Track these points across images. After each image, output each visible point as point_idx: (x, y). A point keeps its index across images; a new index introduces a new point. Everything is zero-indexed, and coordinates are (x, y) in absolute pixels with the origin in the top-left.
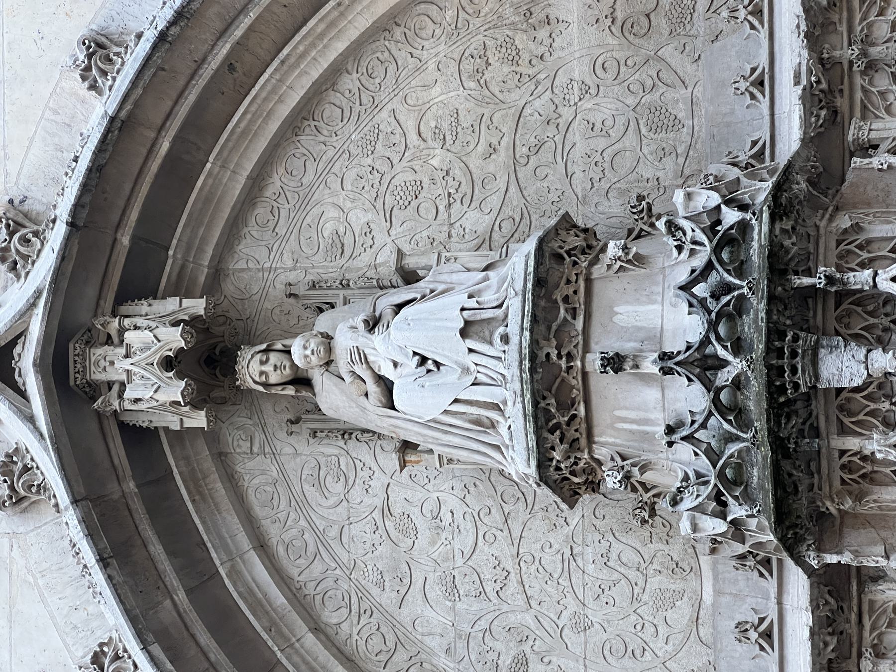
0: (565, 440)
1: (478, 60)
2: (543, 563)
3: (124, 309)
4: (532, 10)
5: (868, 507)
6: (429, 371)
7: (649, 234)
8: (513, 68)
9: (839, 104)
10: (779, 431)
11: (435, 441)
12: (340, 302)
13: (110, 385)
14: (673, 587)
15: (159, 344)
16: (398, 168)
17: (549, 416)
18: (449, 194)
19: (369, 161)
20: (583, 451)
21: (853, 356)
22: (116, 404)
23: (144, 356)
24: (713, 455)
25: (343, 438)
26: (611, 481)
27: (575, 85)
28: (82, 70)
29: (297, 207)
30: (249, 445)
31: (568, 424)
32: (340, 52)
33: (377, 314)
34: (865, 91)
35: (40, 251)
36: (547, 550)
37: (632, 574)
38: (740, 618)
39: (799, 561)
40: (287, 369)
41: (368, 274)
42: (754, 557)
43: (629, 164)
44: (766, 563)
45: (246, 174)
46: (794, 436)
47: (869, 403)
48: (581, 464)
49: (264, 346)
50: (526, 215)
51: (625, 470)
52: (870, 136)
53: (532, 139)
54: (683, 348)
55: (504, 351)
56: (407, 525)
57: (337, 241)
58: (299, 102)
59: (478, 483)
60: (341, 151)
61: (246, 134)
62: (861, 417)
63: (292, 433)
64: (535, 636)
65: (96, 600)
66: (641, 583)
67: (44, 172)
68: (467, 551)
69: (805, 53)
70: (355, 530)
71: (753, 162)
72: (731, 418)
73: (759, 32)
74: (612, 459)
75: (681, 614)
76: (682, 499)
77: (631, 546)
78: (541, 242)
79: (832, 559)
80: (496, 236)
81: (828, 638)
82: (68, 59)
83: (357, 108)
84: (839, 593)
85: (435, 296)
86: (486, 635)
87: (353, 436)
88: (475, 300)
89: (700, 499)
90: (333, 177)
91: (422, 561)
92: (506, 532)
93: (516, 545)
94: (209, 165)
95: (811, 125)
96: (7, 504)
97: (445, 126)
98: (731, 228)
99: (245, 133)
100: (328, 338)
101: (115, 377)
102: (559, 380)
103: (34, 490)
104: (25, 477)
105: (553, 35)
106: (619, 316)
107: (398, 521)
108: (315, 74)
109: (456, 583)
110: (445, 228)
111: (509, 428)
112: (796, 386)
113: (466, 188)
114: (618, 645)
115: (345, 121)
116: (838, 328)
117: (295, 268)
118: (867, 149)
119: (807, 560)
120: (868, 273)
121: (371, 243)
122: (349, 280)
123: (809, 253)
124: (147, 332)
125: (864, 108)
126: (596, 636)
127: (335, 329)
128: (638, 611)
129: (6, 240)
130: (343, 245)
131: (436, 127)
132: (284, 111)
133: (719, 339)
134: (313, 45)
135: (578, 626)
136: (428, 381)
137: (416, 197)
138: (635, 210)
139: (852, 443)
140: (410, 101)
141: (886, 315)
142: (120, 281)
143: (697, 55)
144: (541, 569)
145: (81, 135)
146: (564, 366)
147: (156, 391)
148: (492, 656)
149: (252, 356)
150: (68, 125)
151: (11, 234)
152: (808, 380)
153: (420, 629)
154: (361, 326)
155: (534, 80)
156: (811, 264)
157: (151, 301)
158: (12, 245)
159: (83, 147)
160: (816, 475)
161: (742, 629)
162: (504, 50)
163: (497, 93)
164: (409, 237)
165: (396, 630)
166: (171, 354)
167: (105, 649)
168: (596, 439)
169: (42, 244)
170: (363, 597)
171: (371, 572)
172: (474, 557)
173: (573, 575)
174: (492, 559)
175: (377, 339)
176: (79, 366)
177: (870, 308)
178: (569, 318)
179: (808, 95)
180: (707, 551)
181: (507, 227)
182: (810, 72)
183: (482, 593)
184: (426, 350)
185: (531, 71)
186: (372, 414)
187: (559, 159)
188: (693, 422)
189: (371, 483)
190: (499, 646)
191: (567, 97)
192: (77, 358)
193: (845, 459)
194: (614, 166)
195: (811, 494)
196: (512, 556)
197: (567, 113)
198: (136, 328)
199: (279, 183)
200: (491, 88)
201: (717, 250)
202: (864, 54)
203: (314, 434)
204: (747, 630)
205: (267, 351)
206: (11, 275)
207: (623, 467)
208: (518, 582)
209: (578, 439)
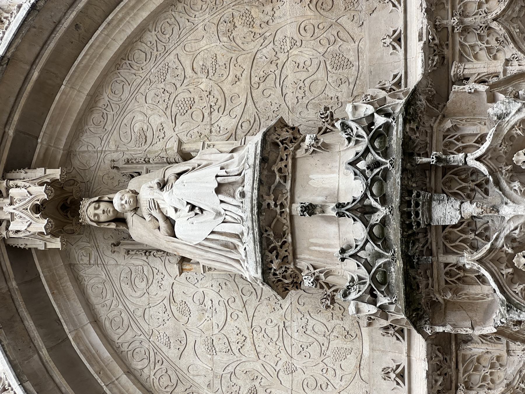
1: (229, 24)
2: (267, 332)
3: (9, 175)
5: (462, 298)
6: (196, 214)
7: (331, 131)
8: (250, 29)
9: (446, 53)
10: (408, 251)
12: (144, 171)
14: (345, 346)
15: (31, 197)
16: (180, 90)
17: (269, 242)
18: (211, 106)
19: (162, 85)
20: (290, 264)
21: (452, 206)
24: (368, 266)
25: (145, 255)
26: (307, 282)
27: (288, 40)
31: (281, 247)
33: (166, 179)
34: (462, 45)
37: (321, 339)
39: (420, 331)
40: (111, 212)
41: (161, 155)
42: (393, 328)
45: (86, 92)
46: (417, 254)
47: (462, 235)
48: (289, 272)
49: (97, 199)
50: (257, 119)
51: (316, 275)
52: (464, 73)
53: (262, 73)
55: (242, 202)
56: (184, 308)
59: (227, 283)
60: (145, 79)
61: (88, 68)
62: (457, 243)
63: (114, 252)
66: (326, 344)
68: (221, 324)
69: (425, 21)
70: (153, 311)
71: (394, 87)
72: (380, 243)
75: (351, 362)
76: (350, 293)
77: (320, 321)
78: (265, 135)
79: (440, 329)
80: (239, 132)
81: (438, 378)
83: (155, 53)
85: (201, 168)
87: (152, 253)
88: (224, 170)
89: (361, 293)
92: (244, 313)
93: (250, 321)
97: (209, 64)
98: (380, 127)
99: (86, 67)
102: (275, 220)
105: (274, 9)
106: (312, 181)
107: (179, 306)
109: (214, 344)
110: (208, 127)
112: (418, 224)
113: (221, 102)
114: (312, 382)
115: (148, 60)
117: (117, 151)
119: (425, 330)
120: (461, 155)
121: (163, 136)
123: (427, 143)
124: (23, 189)
125: (461, 55)
126: (299, 376)
128: (324, 361)
130: (146, 137)
131: (203, 65)
132: (110, 54)
133: (372, 195)
134: (128, 14)
135: (288, 370)
137: (191, 108)
138: (323, 116)
139: (452, 259)
140: (187, 49)
141: (473, 181)
143: (361, 23)
146: (278, 211)
148: (236, 388)
149: (90, 205)
155: (263, 37)
156: (428, 150)
157: (27, 170)
160: (430, 278)
161: (386, 373)
162: (244, 18)
163: (240, 44)
164: (186, 133)
166: (38, 203)
168: (298, 256)
171: (162, 337)
172: (225, 328)
174: (236, 329)
175: (165, 194)
177: (463, 177)
178: (282, 182)
179: (427, 47)
180: (366, 325)
181: (246, 126)
182: (428, 33)
183: (230, 350)
185: (261, 31)
186: (160, 239)
187: (278, 85)
188: (357, 246)
189: (162, 282)
190: (240, 383)
191: (283, 47)
196: (248, 327)
197: (282, 57)
198: (17, 186)
199: (107, 99)
200: (237, 41)
201: (372, 141)
202: (461, 22)
203: (128, 252)
204: (389, 372)
205: (98, 201)
207: (314, 274)
208: (251, 344)
209: (287, 256)
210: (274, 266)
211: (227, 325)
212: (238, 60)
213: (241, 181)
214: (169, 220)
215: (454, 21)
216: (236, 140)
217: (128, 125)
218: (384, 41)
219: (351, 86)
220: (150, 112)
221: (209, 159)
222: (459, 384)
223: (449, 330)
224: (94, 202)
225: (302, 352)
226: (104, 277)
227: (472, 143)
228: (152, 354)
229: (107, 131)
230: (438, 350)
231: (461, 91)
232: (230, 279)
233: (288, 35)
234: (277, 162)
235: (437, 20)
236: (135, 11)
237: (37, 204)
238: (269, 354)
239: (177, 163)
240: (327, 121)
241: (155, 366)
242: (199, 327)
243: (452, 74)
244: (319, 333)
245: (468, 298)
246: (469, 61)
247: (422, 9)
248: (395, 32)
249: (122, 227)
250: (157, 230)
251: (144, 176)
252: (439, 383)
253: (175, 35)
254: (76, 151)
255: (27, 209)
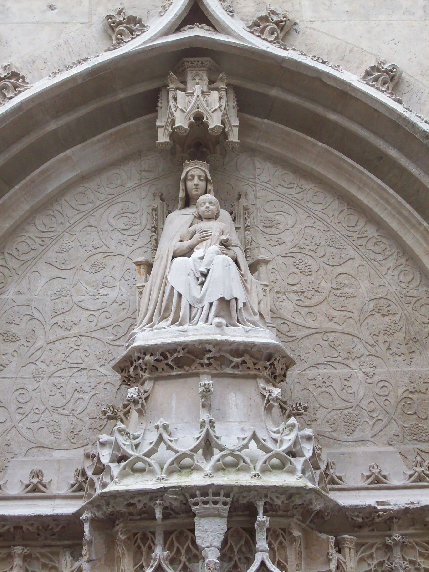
0: (157, 363)
1: (386, 310)
2: (76, 351)
3: (231, 91)
4: (418, 343)
5: (120, 549)
6: (198, 279)
7: (284, 414)
9: (365, 529)
11: (153, 283)
13: (184, 82)
14: (62, 432)
15: (211, 112)
16: (319, 260)
18: (303, 292)
19: (323, 243)
20: (150, 374)
22: (171, 86)
23: (204, 103)
25: (152, 227)
26: (132, 392)
27: (372, 369)
28: (378, 67)
29: (294, 199)
30: (146, 169)
31: (167, 364)
32: (391, 225)
33: (231, 247)
35: (266, 40)
36: (85, 353)
38: (45, 472)
40: (196, 192)
41: (253, 243)
42: (84, 481)
43: (324, 403)
44: (80, 489)
45: (314, 167)
48: (141, 373)
49: (209, 177)
50: (292, 339)
51: (139, 400)
52: (346, 548)
54: (217, 435)
55: (211, 324)
56: (98, 267)
57: (274, 223)
58: (359, 200)
59: (126, 311)
60: (329, 226)
61: (339, 169)
62: (176, 544)
63: (154, 196)
64: (29, 347)
65: (50, 74)
66: (64, 412)
67: (314, 43)
68: (81, 304)
69: (396, 508)
71: (329, 477)
73: (408, 480)
74: (146, 392)
75: (45, 437)
76: (123, 435)
79: (87, 528)
80: (279, 321)
81: (35, 526)
82: (383, 59)
83: (356, 235)
84: (61, 534)
85: (243, 283)
86: (30, 316)
87: (154, 234)
88: (242, 306)
90: (313, 221)
91: (76, 277)
92: (95, 328)
93: (87, 334)
94: (320, 144)
95: (353, 513)
96: (110, 20)
97: (346, 290)
98: (291, 464)
100: (215, 217)
101: (189, 86)
102: (193, 358)
103: (119, 36)
104: (127, 31)
105: (402, 355)
106: (234, 395)
107: (101, 261)
108: (377, 210)
109: (62, 298)
110: (282, 290)
111: (164, 328)
112: (196, 504)
113: (308, 302)
115: (348, 228)
116: (232, 529)
117: (256, 198)
118: (338, 546)
119: (85, 513)
121: (272, 245)
122: (250, 231)
123: (276, 511)
124: (218, 104)
126: (31, 385)
127: (222, 221)
128: (47, 410)
129: (273, 20)
130: (271, 227)
131: (344, 284)
132: (353, 190)
133: (224, 456)
134: (394, 208)
135: (37, 373)
136: (192, 279)
137: (301, 272)
138: (298, 405)
140: (360, 268)
141: (239, 559)
142: (150, 113)
143: (391, 443)
144: (72, 350)
145: (339, 66)
147: (181, 110)
148: (17, 321)
149: (203, 171)
150: (343, 59)
151: (277, 23)
152: (200, 511)
153: (33, 275)
154: (224, 237)
155: (375, 344)
156: (270, 513)
157: (237, 108)
158: (270, 24)
159: (331, 67)
160: (139, 517)
161: (38, 474)
162: (393, 325)
163: (366, 322)
164: (276, 267)
165: (32, 260)
166: (205, 119)
167: (21, 80)
169: (270, 42)
170: (52, 240)
171: (68, 244)
172: (79, 308)
173: (68, 370)
174: (78, 320)
175: (216, 247)
176: (196, 63)
177: (244, 549)
178: (233, 364)
180: (86, 452)
181: (284, 328)
182: (385, 511)
183: (56, 313)
184: (211, 277)
186: (169, 241)
187: (327, 359)
188: (171, 441)
189: (124, 245)
190: (23, 325)
191: (365, 364)
192: (201, 62)
193: (149, 535)
194: (323, 393)
195: (127, 514)
196: (80, 332)
198: (220, 98)
201: (277, 455)
202: (397, 543)
204: (38, 477)
205: (207, 180)
206: (251, 23)
207: (141, 398)
208: (63, 336)
209: (157, 370)
210: (148, 357)
211: (82, 310)
212: (351, 319)
213: (232, 323)
214: (190, 252)
215: (397, 536)
216: (271, 317)
217: (282, 209)
218: (376, 467)
219: (327, 434)
220: (296, 230)
221: (252, 291)
222: (28, 548)
223: (86, 537)
224: (206, 175)
225: (55, 388)
226: (129, 185)
227: (278, 557)
228: (51, 235)
229: (276, 188)
230: (64, 527)
231: (330, 546)
232: (129, 313)
233: (378, 370)
234: (252, 359)
235: (397, 520)
236: (397, 216)
237: (203, 118)
238: (53, 354)
239: (246, 259)
240: (293, 410)
241: (39, 237)
242: (79, 282)
243: (345, 536)
244: (76, 405)
245: (119, 556)
246: (357, 552)
247: (409, 504)
248: (385, 477)
249: (180, 203)
250: (179, 239)
251: (233, 226)
252: (30, 529)
253: (373, 256)
254: (255, 156)
255: (198, 108)
